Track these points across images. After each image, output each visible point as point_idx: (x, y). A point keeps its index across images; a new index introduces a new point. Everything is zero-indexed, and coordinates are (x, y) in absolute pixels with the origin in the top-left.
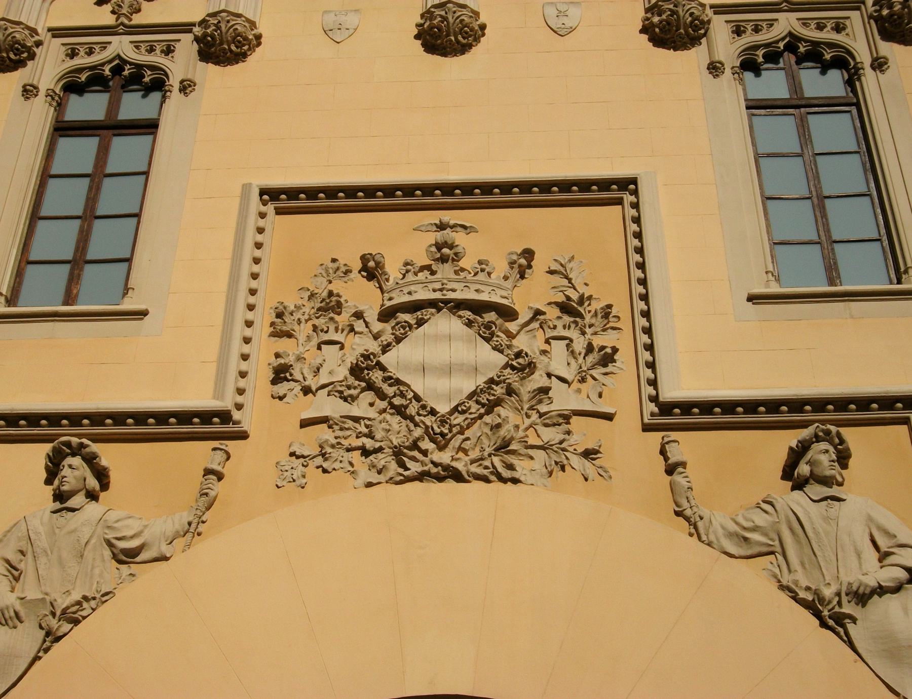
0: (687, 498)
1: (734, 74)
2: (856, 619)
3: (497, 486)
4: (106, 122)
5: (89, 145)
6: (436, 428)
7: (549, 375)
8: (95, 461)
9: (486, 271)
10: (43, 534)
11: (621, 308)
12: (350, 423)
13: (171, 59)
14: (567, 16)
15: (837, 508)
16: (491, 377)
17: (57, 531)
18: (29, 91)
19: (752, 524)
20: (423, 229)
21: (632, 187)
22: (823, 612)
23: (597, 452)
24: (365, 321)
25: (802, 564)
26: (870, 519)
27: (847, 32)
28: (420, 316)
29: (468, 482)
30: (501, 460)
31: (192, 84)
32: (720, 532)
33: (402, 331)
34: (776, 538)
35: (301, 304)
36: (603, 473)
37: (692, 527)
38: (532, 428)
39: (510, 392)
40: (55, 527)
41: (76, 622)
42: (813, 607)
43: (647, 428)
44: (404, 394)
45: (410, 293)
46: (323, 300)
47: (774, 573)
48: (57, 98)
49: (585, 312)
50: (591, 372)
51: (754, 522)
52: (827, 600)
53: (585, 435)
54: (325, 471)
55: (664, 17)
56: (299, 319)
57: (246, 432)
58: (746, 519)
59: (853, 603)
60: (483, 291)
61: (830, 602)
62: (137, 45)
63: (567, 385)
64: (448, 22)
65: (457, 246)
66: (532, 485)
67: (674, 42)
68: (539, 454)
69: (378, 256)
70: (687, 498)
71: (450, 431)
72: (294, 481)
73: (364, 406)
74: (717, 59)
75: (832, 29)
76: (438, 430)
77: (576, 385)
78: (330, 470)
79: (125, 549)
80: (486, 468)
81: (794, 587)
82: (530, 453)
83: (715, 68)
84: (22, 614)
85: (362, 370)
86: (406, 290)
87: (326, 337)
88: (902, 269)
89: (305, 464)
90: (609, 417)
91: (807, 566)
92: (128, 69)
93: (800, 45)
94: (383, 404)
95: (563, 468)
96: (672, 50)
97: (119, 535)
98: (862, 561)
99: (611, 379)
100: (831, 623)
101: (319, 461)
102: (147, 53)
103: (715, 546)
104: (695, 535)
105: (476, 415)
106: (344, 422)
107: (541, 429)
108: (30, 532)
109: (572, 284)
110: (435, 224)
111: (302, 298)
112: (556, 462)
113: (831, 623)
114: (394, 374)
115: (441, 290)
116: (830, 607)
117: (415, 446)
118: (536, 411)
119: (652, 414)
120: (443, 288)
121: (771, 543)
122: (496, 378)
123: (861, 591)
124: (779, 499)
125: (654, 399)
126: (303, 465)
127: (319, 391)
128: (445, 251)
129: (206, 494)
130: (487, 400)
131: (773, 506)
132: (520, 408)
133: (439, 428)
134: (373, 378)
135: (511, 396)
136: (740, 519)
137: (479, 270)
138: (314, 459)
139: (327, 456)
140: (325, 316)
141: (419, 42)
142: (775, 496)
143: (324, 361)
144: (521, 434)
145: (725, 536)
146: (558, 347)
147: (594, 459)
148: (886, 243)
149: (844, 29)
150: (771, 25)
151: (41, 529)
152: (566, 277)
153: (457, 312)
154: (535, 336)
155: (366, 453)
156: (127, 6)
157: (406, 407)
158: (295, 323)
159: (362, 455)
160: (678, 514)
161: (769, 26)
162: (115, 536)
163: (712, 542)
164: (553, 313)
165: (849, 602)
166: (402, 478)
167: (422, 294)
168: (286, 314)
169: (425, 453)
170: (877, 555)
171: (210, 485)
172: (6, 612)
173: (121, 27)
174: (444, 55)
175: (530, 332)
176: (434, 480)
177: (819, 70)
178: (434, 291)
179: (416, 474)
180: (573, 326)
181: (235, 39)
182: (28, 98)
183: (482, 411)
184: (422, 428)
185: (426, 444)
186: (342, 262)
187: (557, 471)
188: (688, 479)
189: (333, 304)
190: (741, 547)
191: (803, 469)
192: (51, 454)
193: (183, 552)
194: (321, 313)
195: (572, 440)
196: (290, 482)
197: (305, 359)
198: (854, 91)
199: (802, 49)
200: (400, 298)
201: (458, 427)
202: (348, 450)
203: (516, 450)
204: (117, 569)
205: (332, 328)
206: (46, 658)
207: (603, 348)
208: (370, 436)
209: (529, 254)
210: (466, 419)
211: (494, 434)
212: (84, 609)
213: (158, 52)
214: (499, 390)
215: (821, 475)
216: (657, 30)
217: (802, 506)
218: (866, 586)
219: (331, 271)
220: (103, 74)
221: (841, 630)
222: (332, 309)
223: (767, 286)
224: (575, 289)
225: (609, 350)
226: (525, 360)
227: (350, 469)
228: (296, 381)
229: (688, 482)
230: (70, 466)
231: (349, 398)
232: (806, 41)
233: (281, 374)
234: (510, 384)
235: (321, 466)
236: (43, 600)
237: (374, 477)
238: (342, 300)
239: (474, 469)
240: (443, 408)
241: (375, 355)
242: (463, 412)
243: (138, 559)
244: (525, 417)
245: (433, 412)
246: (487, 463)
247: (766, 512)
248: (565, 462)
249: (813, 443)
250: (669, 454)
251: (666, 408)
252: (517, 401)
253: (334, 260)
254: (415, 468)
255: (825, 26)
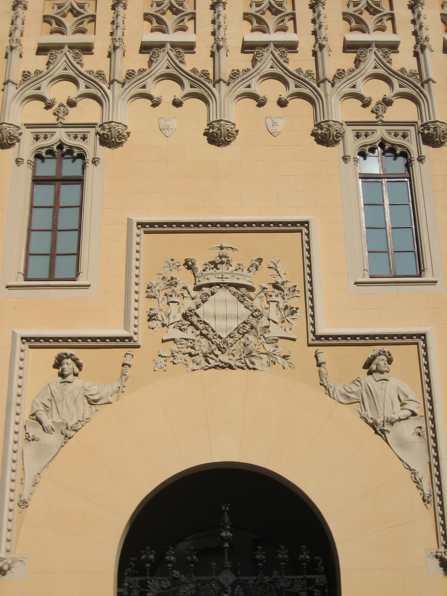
0: (326, 378)
1: (354, 161)
2: (390, 432)
3: (247, 371)
4: (57, 177)
5: (49, 189)
6: (221, 345)
7: (269, 319)
8: (77, 361)
9: (241, 269)
10: (58, 392)
11: (300, 287)
12: (184, 342)
13: (86, 143)
14: (277, 125)
15: (386, 384)
16: (244, 321)
17: (64, 392)
18: (18, 161)
19: (351, 390)
20: (213, 248)
21: (306, 225)
22: (377, 428)
23: (288, 356)
24: (187, 290)
25: (370, 407)
26: (399, 389)
27: (408, 139)
28: (213, 291)
29: (235, 369)
30: (249, 360)
31: (98, 160)
32: (338, 393)
33: (205, 298)
34: (360, 396)
35: (159, 282)
36: (291, 365)
37: (327, 390)
38: (261, 344)
39: (252, 327)
40: (63, 390)
41: (76, 431)
42: (373, 426)
43: (309, 345)
44: (207, 329)
45: (208, 279)
46: (168, 281)
47: (359, 411)
48: (32, 164)
49: (285, 288)
50: (287, 318)
51: (352, 390)
52: (379, 424)
53: (284, 348)
54: (174, 363)
55: (323, 131)
56: (159, 290)
57: (140, 345)
58: (349, 388)
59: (389, 425)
60: (240, 279)
61: (380, 425)
62: (69, 134)
63: (277, 324)
64: (221, 131)
65: (228, 257)
66: (262, 371)
67: (327, 143)
68: (265, 357)
69: (193, 260)
70: (326, 378)
71: (227, 346)
72: (162, 368)
73: (190, 333)
74: (347, 155)
75: (401, 136)
76: (222, 346)
77: (280, 324)
78: (177, 363)
79: (94, 400)
80: (243, 363)
81: (366, 417)
82: (261, 356)
83: (346, 159)
84: (54, 428)
85: (188, 316)
86: (206, 277)
87: (171, 299)
88: (422, 269)
89: (166, 360)
90: (294, 340)
91: (372, 408)
92: (66, 148)
93: (386, 144)
94: (198, 332)
95: (274, 363)
96: (325, 146)
97: (91, 394)
98: (394, 407)
99: (295, 321)
100: (379, 432)
101: (172, 359)
102: (74, 139)
103: (336, 399)
104: (328, 394)
105: (238, 339)
106: (181, 341)
107: (266, 345)
108: (52, 391)
109: (279, 274)
110: (219, 247)
111: (159, 278)
112: (272, 361)
113: (379, 432)
114: (202, 319)
115: (222, 278)
116: (380, 426)
117: (212, 352)
118: (263, 336)
119: (312, 340)
120: (223, 277)
121: (359, 398)
122: (246, 321)
123: (392, 421)
124: (363, 380)
125: (314, 333)
126: (165, 361)
127: (170, 326)
128: (224, 259)
129: (125, 375)
130: (243, 332)
131: (360, 383)
132: (256, 335)
133: (223, 345)
134: (193, 320)
135: (252, 329)
136: (347, 388)
137: (238, 268)
138: (169, 358)
139: (175, 357)
140: (170, 288)
141: (206, 137)
142: (362, 378)
143: (171, 311)
144: (257, 347)
145: (340, 395)
146: (273, 305)
147: (287, 359)
148: (416, 253)
149: (407, 136)
150: (374, 133)
151: (57, 390)
152: (277, 270)
153: (228, 288)
154: (263, 300)
155: (191, 355)
156: (62, 112)
157: (208, 334)
158: (157, 291)
159: (189, 356)
160: (321, 384)
161: (372, 133)
162: (89, 394)
163: (335, 398)
164: (270, 288)
165: (387, 425)
166: (207, 367)
167: (213, 280)
168: (153, 287)
169: (217, 356)
170: (400, 403)
171: (127, 371)
172: (48, 428)
173: (60, 124)
174: (219, 146)
175: (261, 298)
176: (221, 369)
177: (393, 157)
178: (219, 278)
179: (213, 366)
180: (279, 295)
181: (118, 136)
182: (19, 165)
183: (241, 336)
184: (215, 344)
185: (217, 352)
186: (176, 260)
187: (272, 365)
188: (326, 370)
189: (174, 283)
190: (346, 399)
191: (374, 367)
192: (57, 357)
193: (117, 400)
194: (168, 286)
195: (278, 350)
196: (160, 368)
197: (163, 310)
198: (409, 170)
199: (387, 147)
200: (204, 282)
201: (231, 344)
202: (184, 354)
203: (255, 355)
204: (90, 407)
205: (174, 295)
206: (66, 446)
207: (292, 308)
208: (193, 348)
209: (260, 260)
210: (234, 340)
211: (246, 348)
212: (79, 425)
213: (79, 138)
214: (248, 327)
215: (380, 370)
216: (320, 137)
217: (372, 383)
218: (395, 419)
219: (171, 265)
220: (53, 150)
221: (383, 436)
222: (173, 285)
223: (364, 277)
224: (280, 276)
225: (295, 309)
226: (259, 313)
227: (185, 362)
228: (159, 320)
229: (326, 371)
230: (67, 363)
231: (183, 330)
232: (389, 143)
233: (151, 318)
234: (252, 324)
235: (173, 361)
236: (63, 423)
237: (196, 367)
238: (177, 281)
239: (238, 364)
240: (224, 335)
241: (194, 310)
242: (233, 337)
243: (98, 403)
244: (258, 339)
245: (220, 337)
246: (243, 361)
247: (357, 385)
248: (276, 361)
249: (378, 356)
250: (319, 358)
251: (318, 338)
252: (255, 332)
253: (172, 260)
254: (213, 363)
255: (398, 135)
